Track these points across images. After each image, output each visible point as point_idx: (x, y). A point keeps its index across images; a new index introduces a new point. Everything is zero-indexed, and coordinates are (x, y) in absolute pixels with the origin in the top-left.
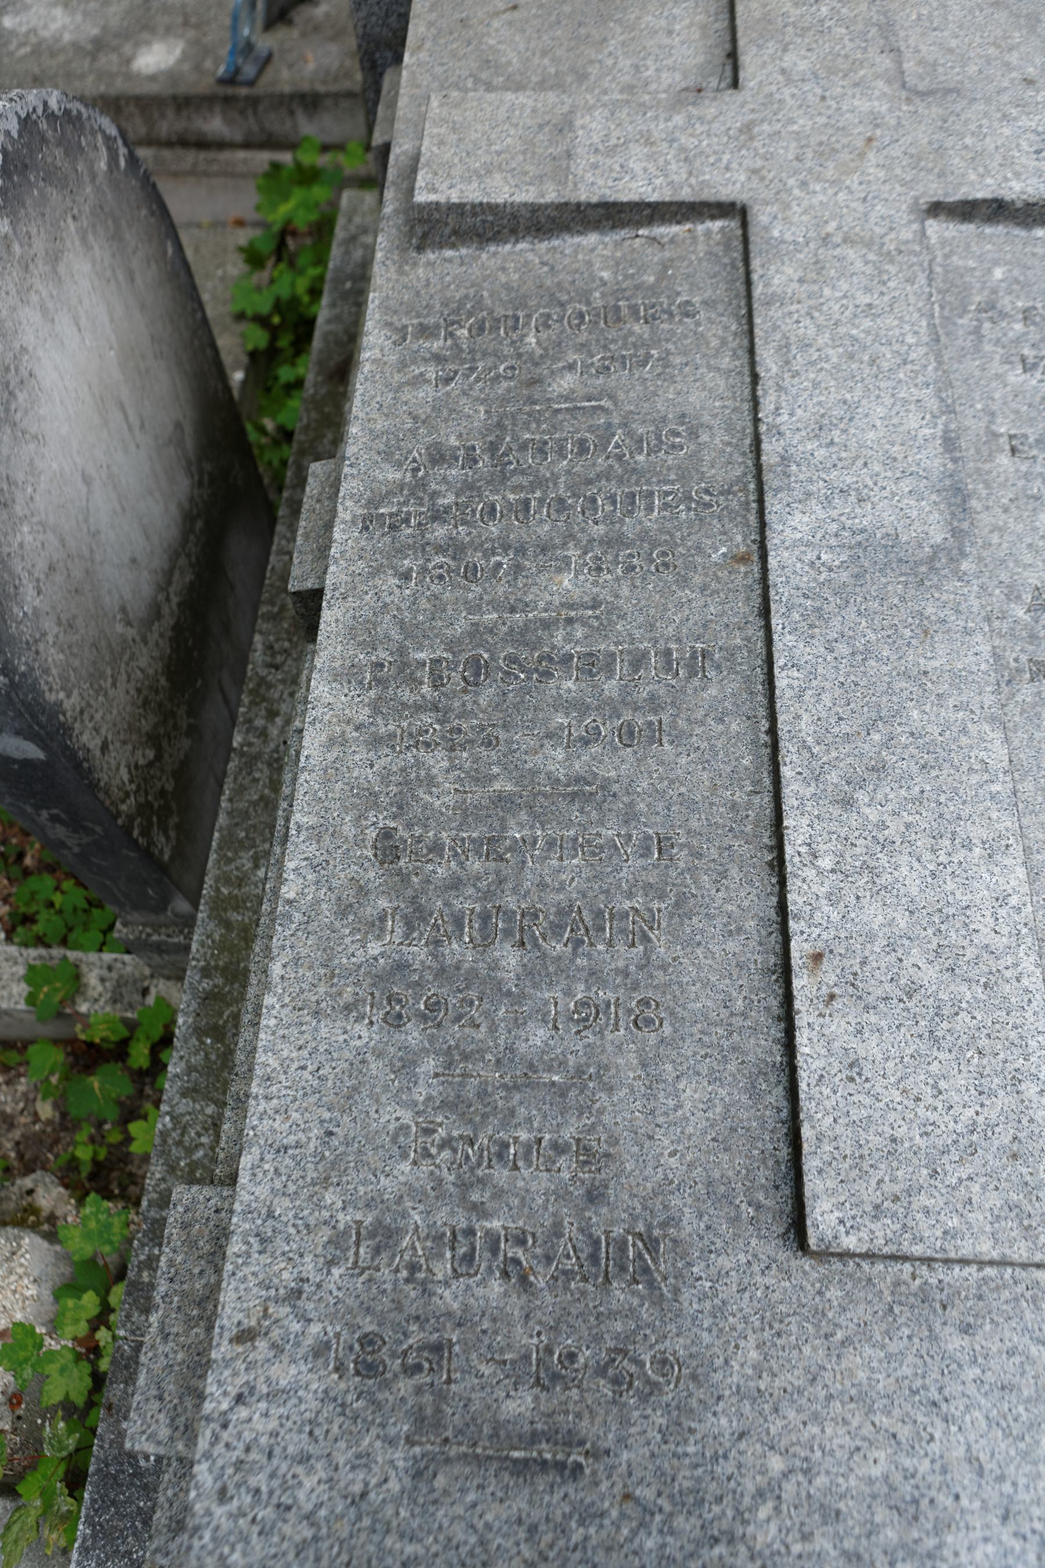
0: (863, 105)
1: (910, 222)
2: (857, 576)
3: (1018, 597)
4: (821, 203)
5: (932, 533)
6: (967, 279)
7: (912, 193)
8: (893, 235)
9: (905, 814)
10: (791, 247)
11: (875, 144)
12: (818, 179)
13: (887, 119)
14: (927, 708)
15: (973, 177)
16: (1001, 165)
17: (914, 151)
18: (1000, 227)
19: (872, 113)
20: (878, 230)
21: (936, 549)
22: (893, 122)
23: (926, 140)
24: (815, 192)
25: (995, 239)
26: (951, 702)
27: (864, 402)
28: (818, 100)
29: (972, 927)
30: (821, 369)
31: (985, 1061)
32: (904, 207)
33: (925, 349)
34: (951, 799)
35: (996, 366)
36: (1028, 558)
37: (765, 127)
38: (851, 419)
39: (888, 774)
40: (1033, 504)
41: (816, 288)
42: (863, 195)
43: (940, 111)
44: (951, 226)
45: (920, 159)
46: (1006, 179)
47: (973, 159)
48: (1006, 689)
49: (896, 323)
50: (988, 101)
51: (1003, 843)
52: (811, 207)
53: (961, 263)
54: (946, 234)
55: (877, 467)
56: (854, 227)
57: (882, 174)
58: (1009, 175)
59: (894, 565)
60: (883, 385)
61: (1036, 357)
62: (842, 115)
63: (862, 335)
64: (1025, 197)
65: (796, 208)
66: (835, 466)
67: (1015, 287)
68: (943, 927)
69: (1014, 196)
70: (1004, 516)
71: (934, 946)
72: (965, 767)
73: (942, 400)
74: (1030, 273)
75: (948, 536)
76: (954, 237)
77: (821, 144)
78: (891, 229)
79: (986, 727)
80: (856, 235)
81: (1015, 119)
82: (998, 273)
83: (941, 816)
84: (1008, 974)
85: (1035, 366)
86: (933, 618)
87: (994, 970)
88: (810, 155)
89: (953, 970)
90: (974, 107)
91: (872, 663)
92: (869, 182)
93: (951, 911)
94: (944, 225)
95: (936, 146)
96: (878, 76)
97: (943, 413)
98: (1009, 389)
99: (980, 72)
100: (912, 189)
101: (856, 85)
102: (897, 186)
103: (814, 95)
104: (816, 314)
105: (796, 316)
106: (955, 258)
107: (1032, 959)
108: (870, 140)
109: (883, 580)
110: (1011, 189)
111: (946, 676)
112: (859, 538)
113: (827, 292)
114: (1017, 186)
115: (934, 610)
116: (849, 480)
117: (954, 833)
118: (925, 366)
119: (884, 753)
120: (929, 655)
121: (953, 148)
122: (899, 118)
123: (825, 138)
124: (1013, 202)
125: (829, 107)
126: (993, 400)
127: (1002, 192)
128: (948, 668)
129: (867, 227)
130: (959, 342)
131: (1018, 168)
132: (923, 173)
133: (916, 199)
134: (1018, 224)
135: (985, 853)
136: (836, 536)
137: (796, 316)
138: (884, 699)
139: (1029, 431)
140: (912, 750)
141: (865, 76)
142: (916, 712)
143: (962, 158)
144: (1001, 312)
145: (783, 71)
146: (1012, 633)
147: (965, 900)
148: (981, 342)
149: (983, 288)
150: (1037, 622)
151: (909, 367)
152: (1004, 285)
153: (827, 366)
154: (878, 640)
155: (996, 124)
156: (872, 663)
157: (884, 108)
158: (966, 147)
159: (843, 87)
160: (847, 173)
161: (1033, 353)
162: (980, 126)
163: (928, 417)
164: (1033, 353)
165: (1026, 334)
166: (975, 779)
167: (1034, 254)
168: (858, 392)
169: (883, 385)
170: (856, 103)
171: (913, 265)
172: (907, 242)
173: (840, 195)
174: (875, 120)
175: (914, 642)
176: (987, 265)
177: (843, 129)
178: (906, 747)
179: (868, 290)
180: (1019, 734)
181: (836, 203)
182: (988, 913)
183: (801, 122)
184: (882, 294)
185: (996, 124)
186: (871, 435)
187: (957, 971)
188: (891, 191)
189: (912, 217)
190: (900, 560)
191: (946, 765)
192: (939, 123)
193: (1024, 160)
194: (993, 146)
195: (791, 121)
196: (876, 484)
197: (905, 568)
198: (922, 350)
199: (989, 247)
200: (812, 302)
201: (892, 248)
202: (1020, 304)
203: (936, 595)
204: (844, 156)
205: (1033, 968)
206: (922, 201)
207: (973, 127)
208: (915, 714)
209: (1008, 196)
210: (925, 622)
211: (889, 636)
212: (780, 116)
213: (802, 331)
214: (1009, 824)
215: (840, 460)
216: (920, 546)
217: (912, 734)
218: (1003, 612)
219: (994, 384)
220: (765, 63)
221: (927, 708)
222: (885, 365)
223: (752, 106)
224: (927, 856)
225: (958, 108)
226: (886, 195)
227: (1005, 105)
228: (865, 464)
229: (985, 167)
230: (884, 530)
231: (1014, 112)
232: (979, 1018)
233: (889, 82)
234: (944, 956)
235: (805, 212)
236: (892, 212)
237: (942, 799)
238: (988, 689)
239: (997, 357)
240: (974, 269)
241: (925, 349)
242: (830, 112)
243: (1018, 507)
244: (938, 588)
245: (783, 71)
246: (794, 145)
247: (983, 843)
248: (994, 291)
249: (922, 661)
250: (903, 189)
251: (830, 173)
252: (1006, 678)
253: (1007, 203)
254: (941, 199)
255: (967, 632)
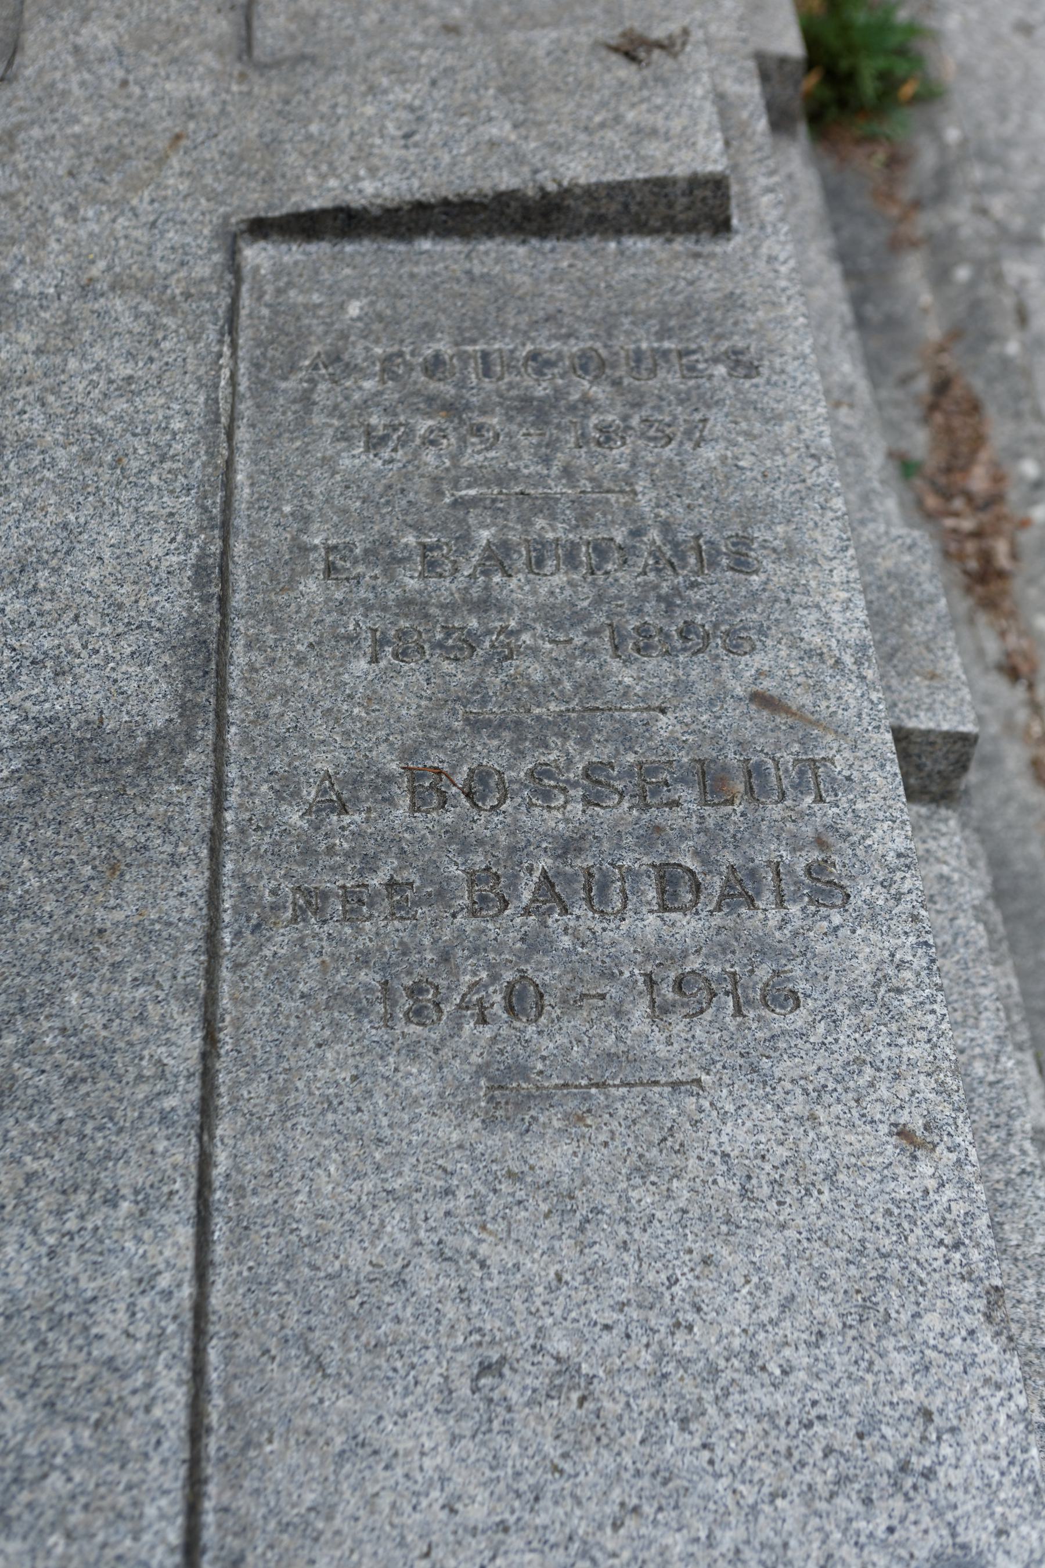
0: (177, 88)
1: (211, 251)
2: (30, 792)
3: (296, 794)
4: (91, 234)
5: (151, 714)
6: (306, 322)
7: (222, 210)
8: (182, 274)
9: (28, 1159)
10: (36, 303)
11: (184, 142)
12: (94, 200)
13: (208, 105)
14: (93, 988)
15: (311, 179)
16: (352, 159)
17: (236, 149)
18: (366, 242)
19: (189, 99)
20: (162, 267)
21: (154, 737)
22: (215, 110)
23: (256, 131)
24: (85, 220)
25: (358, 259)
26: (130, 973)
27: (93, 524)
28: (116, 87)
29: (95, 1331)
30: (41, 480)
31: (74, 1549)
32: (206, 232)
33: (196, 436)
34: (101, 1128)
35: (326, 446)
36: (320, 732)
37: (36, 132)
38: (68, 553)
39: (16, 1099)
40: (344, 647)
41: (58, 360)
42: (152, 218)
43: (284, 89)
44: (294, 248)
45: (242, 159)
46: (357, 178)
47: (316, 153)
48: (250, 939)
49: (162, 401)
50: (351, 69)
51: (165, 1189)
52: (76, 241)
53: (300, 299)
54: (286, 259)
55: (92, 620)
56: (130, 267)
57: (184, 186)
58: (362, 172)
59: (88, 769)
60: (124, 495)
61: (385, 426)
62: (145, 105)
63: (110, 424)
64: (379, 201)
65: (54, 246)
66: (32, 624)
67: (376, 326)
68: (51, 1336)
69: (363, 202)
70: (295, 672)
71: (30, 1369)
72: (131, 1077)
73: (205, 510)
74: (401, 305)
75: (174, 715)
76: (296, 263)
77: (107, 149)
78: (182, 264)
79: (174, 1007)
80: (131, 276)
81: (385, 92)
82: (354, 309)
83: (81, 1156)
84: (134, 1402)
85: (384, 439)
86: (129, 844)
87: (115, 1397)
88: (89, 165)
89: (53, 1405)
90: (331, 80)
91: (27, 924)
92: (165, 198)
93: (68, 1307)
94: (284, 247)
95: (267, 139)
96: (206, 46)
97: (202, 529)
98: (338, 477)
99: (382, 21)
100: (223, 203)
101: (174, 61)
102: (203, 201)
103: (113, 80)
104: (51, 399)
105: (20, 404)
106: (292, 293)
107: (173, 1374)
108: (178, 137)
109: (67, 793)
110: (360, 191)
111: (131, 933)
112: (44, 732)
113: (73, 364)
114: (369, 187)
115: (132, 832)
116: (47, 644)
117: (95, 1183)
118: (191, 462)
119: (16, 1065)
120: (112, 902)
121: (291, 140)
122: (224, 102)
123: (114, 141)
124: (365, 209)
125: (129, 96)
126: (311, 496)
127: (348, 197)
128: (136, 920)
129: (148, 264)
130: (277, 416)
131: (376, 161)
132: (242, 180)
133: (226, 217)
134: (390, 236)
135: (135, 1209)
136: (12, 732)
137: (20, 404)
138: (33, 980)
139: (357, 537)
140: (59, 1056)
141: (189, 47)
142: (75, 995)
143: (301, 153)
144: (347, 365)
145: (76, 50)
146: (276, 853)
147: (89, 1288)
148: (310, 412)
149: (326, 333)
150: (317, 829)
151: (167, 465)
152: (360, 324)
153: (50, 475)
154: (41, 888)
155: (357, 101)
156: (27, 924)
157: (208, 89)
158: (309, 137)
159: (155, 65)
160: (135, 189)
161: (385, 420)
162: (335, 106)
163: (180, 537)
164: (385, 420)
165: (380, 393)
166: (142, 1091)
167: (412, 276)
168: (87, 511)
169: (124, 495)
170: (168, 86)
171: (204, 313)
172: (202, 280)
173: (121, 220)
174: (190, 109)
175: (94, 885)
176: (338, 299)
177: (143, 126)
178: (51, 1051)
179: (131, 356)
180: (259, 1007)
181: (112, 233)
182: (122, 1306)
183: (86, 119)
184: (151, 360)
185: (357, 101)
186: (94, 573)
187: (60, 1406)
188: (190, 212)
189: (215, 245)
190: (98, 761)
191: (105, 1074)
192: (279, 106)
193: (386, 150)
194: (347, 132)
195: (74, 120)
196: (85, 647)
197: (102, 772)
198: (189, 439)
199: (348, 271)
200: (47, 382)
201: (178, 291)
202: (378, 350)
203: (140, 809)
204: (138, 164)
205: (172, 1387)
206: (233, 220)
207: (324, 108)
208: (74, 999)
209: (356, 201)
210: (117, 853)
211: (59, 880)
212: (59, 115)
213: (23, 427)
214: (179, 1158)
215: (40, 614)
216: (132, 735)
217: (63, 1030)
218: (266, 818)
219: (317, 473)
220: (53, 40)
221: (93, 988)
222: (134, 465)
223: (22, 103)
224: (50, 1223)
225: (308, 83)
226: (185, 216)
227: (374, 72)
228: (76, 617)
229: (330, 164)
230: (83, 717)
231: (385, 82)
232: (78, 1478)
233: (220, 53)
234: (45, 1383)
235: (66, 250)
236: (189, 239)
237: (88, 1130)
238: (189, 947)
239: (330, 432)
240: (320, 306)
241: (196, 436)
242: (129, 103)
243: (320, 656)
244: (144, 797)
245: (76, 50)
246: (71, 152)
247: (137, 1192)
248: (344, 336)
249: (100, 913)
250: (212, 205)
251: (113, 191)
252: (254, 922)
253: (357, 211)
254: (262, 214)
255: (175, 861)
